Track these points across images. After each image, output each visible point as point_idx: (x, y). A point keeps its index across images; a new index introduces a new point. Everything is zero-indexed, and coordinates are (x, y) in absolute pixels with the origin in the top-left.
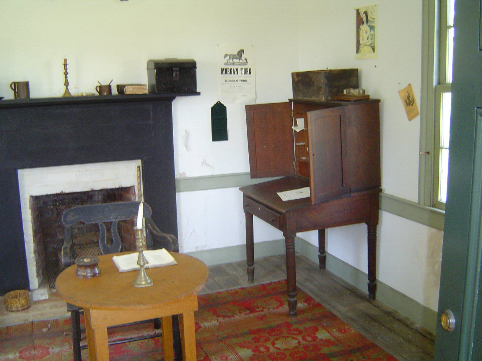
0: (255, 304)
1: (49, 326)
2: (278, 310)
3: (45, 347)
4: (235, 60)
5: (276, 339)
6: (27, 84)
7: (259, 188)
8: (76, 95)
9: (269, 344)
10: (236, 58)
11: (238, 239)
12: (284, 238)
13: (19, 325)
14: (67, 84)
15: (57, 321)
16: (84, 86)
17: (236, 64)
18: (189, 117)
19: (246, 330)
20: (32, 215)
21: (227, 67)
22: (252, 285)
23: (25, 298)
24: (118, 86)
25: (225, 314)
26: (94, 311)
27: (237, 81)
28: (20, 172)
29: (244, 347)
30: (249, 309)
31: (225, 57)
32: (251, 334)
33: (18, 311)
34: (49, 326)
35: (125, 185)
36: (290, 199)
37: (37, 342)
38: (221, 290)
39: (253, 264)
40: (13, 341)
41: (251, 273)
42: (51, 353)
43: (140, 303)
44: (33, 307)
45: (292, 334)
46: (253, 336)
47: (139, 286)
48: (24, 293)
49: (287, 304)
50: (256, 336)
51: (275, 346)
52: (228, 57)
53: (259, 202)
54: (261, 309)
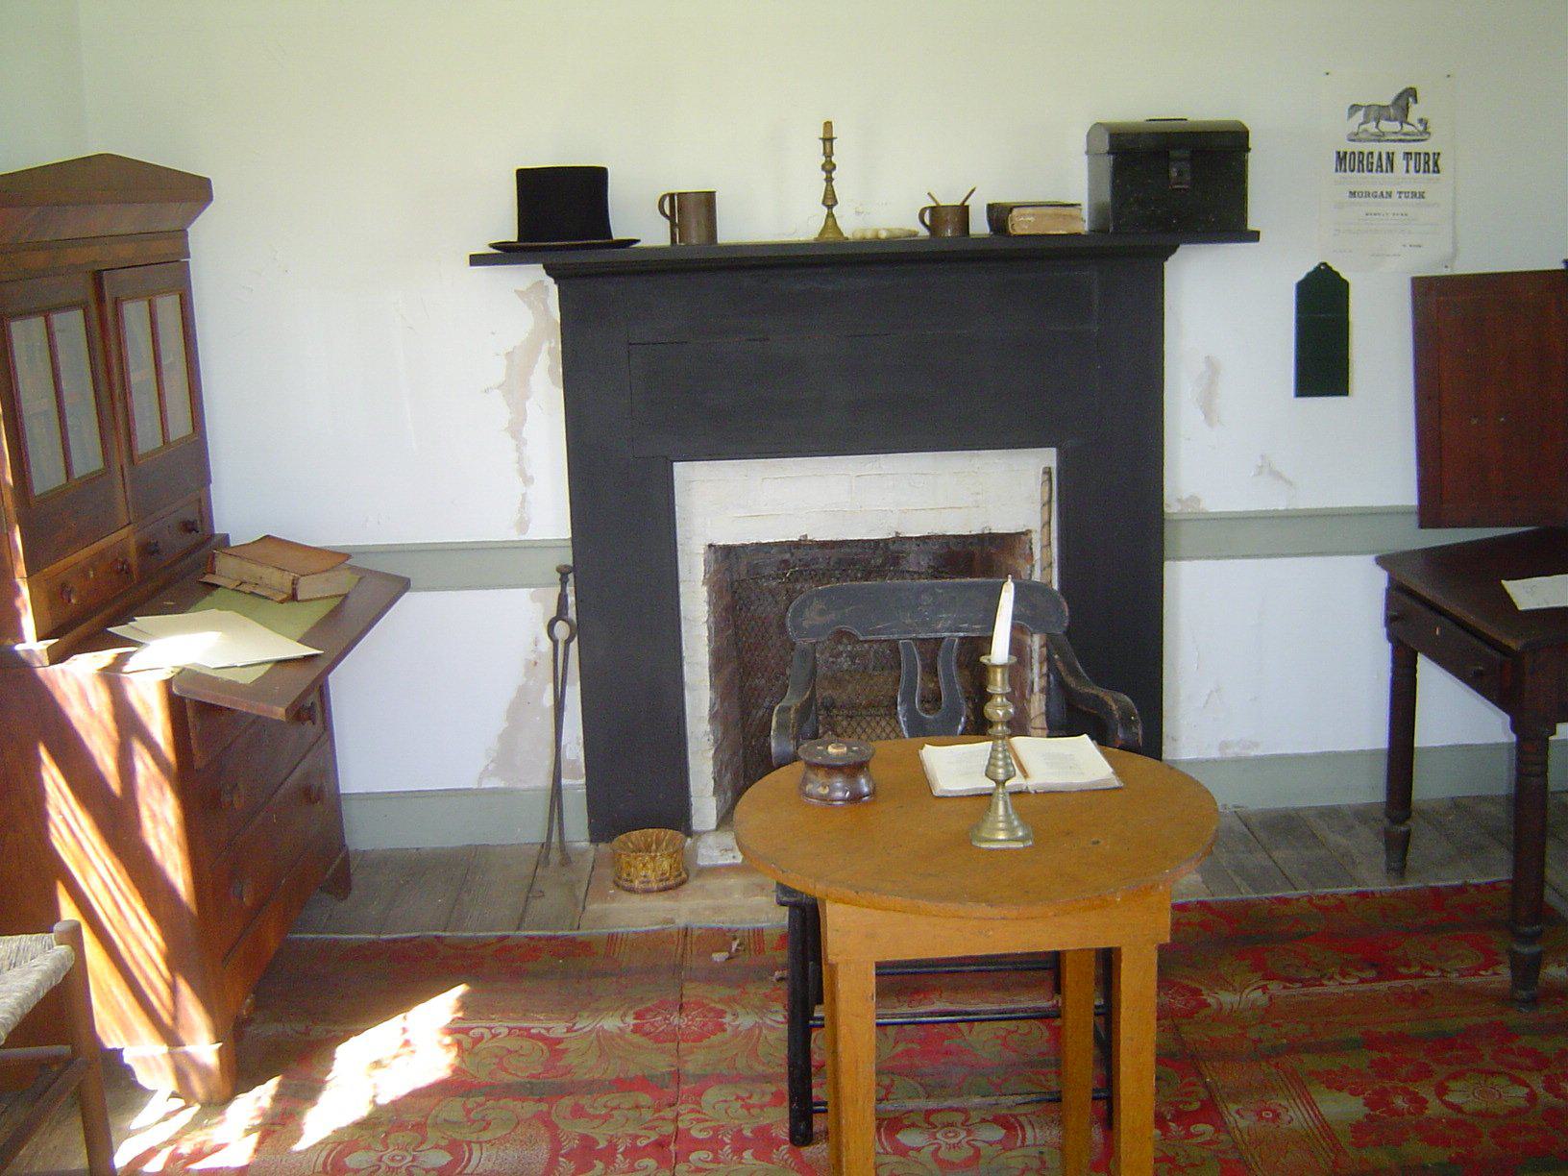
0: (1398, 952)
1: (734, 946)
2: (1474, 980)
3: (712, 1009)
4: (1385, 126)
5: (1455, 1077)
6: (709, 199)
7: (1437, 559)
8: (858, 236)
9: (1425, 1090)
10: (1389, 119)
11: (1368, 730)
12: (1513, 738)
13: (647, 933)
14: (830, 200)
15: (759, 933)
16: (884, 206)
17: (1391, 135)
18: (1221, 315)
19: (1355, 1034)
21: (1357, 147)
22: (1400, 887)
23: (670, 856)
24: (991, 208)
25: (1292, 972)
26: (841, 906)
27: (1390, 195)
28: (679, 468)
29: (1340, 1089)
30: (1373, 966)
31: (1350, 115)
32: (1370, 1048)
34: (734, 946)
35: (1001, 527)
36: (1545, 606)
37: (692, 991)
38: (1290, 893)
39: (1408, 817)
40: (623, 981)
41: (1398, 847)
43: (976, 898)
45: (1512, 1066)
46: (1376, 1055)
47: (984, 845)
48: (671, 840)
49: (1506, 958)
50: (1387, 1055)
51: (1446, 1098)
52: (1360, 114)
53: (1436, 613)
54: (1415, 970)
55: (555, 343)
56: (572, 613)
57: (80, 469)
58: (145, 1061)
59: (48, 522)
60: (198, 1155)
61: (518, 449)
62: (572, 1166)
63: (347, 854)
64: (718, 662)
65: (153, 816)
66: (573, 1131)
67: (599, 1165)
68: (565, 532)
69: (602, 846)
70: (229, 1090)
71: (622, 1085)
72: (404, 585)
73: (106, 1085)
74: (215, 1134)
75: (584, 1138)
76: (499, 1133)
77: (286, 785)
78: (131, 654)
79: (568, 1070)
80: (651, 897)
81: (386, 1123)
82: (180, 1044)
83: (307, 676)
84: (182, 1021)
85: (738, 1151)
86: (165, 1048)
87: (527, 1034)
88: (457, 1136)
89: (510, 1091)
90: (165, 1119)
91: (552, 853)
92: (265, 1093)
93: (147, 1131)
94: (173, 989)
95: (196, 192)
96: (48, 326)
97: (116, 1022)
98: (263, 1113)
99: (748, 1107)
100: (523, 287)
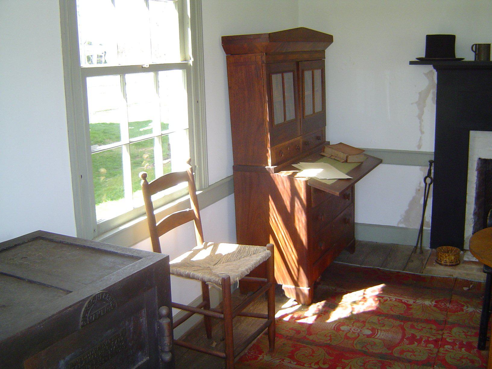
20: (477, 177)
23: (455, 255)
28: (472, 133)
33: (446, 265)
34: (471, 286)
37: (455, 298)
42: (465, 311)
44: (461, 265)
55: (434, 90)
56: (432, 176)
57: (288, 119)
58: (288, 289)
59: (279, 133)
60: (299, 318)
61: (420, 123)
62: (408, 342)
63: (354, 241)
64: (478, 198)
65: (299, 219)
66: (409, 332)
67: (416, 343)
68: (433, 150)
69: (433, 249)
70: (310, 302)
71: (427, 321)
72: (380, 162)
73: (277, 294)
74: (306, 314)
75: (413, 335)
76: (387, 328)
77: (339, 217)
78: (297, 172)
79: (412, 314)
80: (447, 267)
81: (353, 319)
82: (299, 286)
83: (348, 184)
84: (300, 279)
85: (460, 348)
86: (294, 287)
87: (401, 301)
88: (375, 327)
89: (392, 317)
90: (292, 306)
91: (418, 250)
92: (320, 305)
93: (286, 310)
94: (298, 270)
95: (328, 39)
96: (282, 75)
97: (280, 275)
98: (319, 310)
99: (466, 335)
100: (426, 72)
